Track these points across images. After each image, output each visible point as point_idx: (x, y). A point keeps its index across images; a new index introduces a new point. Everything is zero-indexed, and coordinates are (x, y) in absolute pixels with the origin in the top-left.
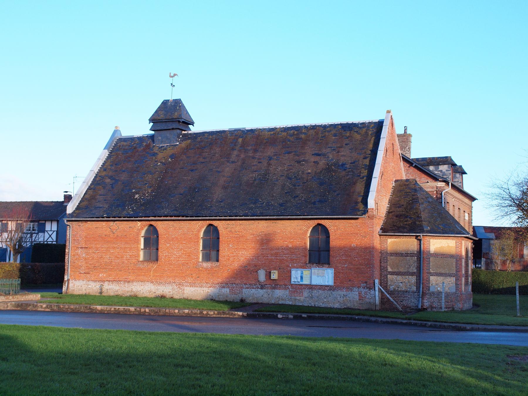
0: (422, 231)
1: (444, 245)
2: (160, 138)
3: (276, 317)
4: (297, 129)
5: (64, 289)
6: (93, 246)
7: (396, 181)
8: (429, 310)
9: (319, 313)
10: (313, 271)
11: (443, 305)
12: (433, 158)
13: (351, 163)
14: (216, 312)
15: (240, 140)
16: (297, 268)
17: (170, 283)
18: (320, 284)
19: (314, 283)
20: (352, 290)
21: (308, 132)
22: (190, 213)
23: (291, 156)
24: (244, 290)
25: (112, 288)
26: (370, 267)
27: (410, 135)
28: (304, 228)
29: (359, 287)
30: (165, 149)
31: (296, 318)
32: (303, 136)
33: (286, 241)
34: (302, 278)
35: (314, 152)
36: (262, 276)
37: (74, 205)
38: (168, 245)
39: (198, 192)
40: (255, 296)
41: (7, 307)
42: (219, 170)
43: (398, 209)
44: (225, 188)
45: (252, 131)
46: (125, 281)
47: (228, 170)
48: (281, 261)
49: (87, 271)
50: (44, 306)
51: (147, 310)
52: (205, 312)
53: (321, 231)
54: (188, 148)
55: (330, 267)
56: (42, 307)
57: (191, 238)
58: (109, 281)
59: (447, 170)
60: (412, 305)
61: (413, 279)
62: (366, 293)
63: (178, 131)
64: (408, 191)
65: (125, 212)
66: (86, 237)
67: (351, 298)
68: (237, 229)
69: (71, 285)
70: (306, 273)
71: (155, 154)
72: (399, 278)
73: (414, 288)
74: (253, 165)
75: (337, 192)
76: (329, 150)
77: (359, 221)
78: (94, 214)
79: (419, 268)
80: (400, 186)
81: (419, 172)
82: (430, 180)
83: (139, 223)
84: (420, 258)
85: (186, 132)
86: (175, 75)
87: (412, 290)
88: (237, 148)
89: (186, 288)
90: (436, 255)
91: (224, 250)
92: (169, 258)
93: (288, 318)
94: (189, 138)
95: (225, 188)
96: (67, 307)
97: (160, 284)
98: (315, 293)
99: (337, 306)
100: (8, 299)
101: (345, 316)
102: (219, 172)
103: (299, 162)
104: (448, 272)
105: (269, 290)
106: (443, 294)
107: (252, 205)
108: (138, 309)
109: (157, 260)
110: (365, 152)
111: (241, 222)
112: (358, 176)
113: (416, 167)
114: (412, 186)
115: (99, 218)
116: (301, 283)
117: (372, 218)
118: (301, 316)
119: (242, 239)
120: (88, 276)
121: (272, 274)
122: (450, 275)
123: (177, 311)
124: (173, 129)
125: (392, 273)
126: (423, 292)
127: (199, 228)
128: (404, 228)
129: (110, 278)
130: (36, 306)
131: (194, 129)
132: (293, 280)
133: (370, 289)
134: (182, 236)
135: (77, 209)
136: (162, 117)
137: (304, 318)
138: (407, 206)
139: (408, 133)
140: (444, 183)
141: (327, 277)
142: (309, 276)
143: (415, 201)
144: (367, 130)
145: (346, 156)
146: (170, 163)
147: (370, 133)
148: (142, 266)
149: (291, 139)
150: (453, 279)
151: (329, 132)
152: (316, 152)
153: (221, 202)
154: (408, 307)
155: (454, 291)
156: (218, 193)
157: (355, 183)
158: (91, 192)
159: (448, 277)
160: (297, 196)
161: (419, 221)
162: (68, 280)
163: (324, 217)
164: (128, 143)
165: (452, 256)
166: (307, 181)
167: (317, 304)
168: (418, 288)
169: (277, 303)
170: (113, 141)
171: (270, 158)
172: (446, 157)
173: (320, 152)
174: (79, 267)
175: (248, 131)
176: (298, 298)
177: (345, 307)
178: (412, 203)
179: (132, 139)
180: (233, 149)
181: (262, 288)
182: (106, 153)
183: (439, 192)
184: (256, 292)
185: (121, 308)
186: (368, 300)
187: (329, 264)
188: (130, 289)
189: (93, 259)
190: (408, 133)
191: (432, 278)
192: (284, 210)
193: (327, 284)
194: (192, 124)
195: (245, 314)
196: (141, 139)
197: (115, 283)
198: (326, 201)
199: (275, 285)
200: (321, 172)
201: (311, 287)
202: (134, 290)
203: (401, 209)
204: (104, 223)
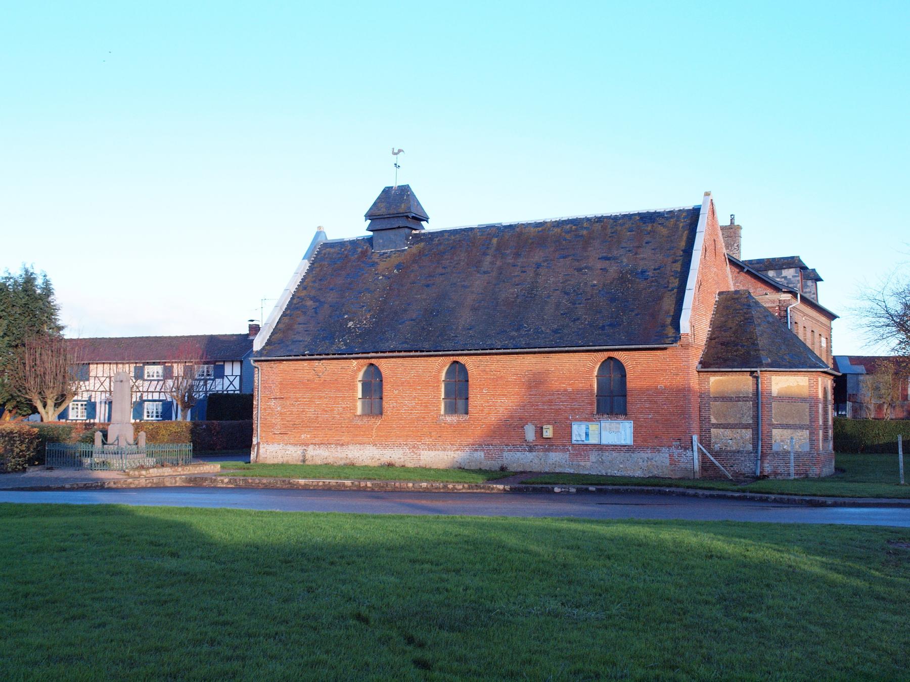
0: (760, 364)
3: (551, 492)
4: (576, 223)
5: (253, 456)
6: (292, 395)
7: (720, 294)
8: (772, 477)
12: (774, 259)
14: (466, 486)
15: (495, 241)
18: (614, 443)
19: (604, 442)
20: (659, 451)
23: (568, 261)
25: (319, 454)
27: (739, 227)
28: (589, 364)
30: (389, 257)
31: (580, 492)
32: (585, 232)
34: (587, 435)
36: (530, 433)
37: (264, 339)
38: (396, 392)
39: (436, 315)
41: (176, 482)
42: (466, 283)
44: (474, 309)
45: (511, 227)
46: (337, 444)
47: (478, 282)
49: (283, 431)
50: (226, 480)
52: (450, 486)
53: (614, 368)
54: (421, 253)
56: (222, 482)
58: (315, 444)
61: (748, 434)
62: (679, 455)
63: (407, 230)
66: (281, 383)
67: (658, 462)
69: (262, 451)
70: (593, 427)
72: (728, 432)
73: (750, 447)
76: (622, 251)
79: (756, 418)
80: (727, 300)
81: (753, 280)
82: (769, 291)
83: (355, 362)
84: (758, 403)
85: (417, 232)
86: (400, 151)
88: (491, 251)
90: (781, 398)
91: (476, 398)
93: (568, 493)
95: (474, 309)
97: (385, 447)
98: (607, 456)
99: (638, 474)
102: (464, 287)
105: (541, 454)
108: (356, 483)
110: (675, 254)
111: (498, 357)
113: (748, 272)
114: (744, 301)
115: (315, 353)
118: (587, 489)
119: (501, 381)
120: (286, 437)
121: (544, 431)
122: (801, 427)
123: (410, 485)
124: (399, 227)
127: (437, 368)
128: (734, 360)
129: (316, 440)
131: (428, 227)
132: (574, 438)
133: (686, 449)
136: (383, 211)
137: (592, 492)
139: (736, 224)
140: (790, 295)
142: (597, 432)
144: (677, 221)
145: (648, 259)
146: (396, 275)
147: (681, 225)
148: (360, 423)
149: (568, 237)
150: (806, 433)
151: (622, 225)
152: (605, 255)
153: (470, 329)
155: (808, 449)
156: (465, 318)
157: (660, 298)
160: (578, 319)
161: (756, 350)
162: (258, 444)
163: (633, 347)
164: (337, 249)
166: (592, 295)
167: (610, 472)
168: (755, 446)
171: (538, 266)
173: (610, 255)
174: (273, 426)
175: (506, 227)
176: (582, 463)
180: (485, 254)
181: (530, 451)
182: (306, 265)
184: (523, 456)
185: (333, 482)
186: (682, 465)
187: (626, 414)
188: (344, 455)
189: (291, 414)
190: (736, 224)
191: (775, 432)
192: (560, 338)
193: (623, 443)
194: (426, 219)
195: (507, 487)
196: (354, 243)
197: (322, 447)
199: (549, 445)
200: (611, 283)
202: (350, 456)
204: (305, 364)
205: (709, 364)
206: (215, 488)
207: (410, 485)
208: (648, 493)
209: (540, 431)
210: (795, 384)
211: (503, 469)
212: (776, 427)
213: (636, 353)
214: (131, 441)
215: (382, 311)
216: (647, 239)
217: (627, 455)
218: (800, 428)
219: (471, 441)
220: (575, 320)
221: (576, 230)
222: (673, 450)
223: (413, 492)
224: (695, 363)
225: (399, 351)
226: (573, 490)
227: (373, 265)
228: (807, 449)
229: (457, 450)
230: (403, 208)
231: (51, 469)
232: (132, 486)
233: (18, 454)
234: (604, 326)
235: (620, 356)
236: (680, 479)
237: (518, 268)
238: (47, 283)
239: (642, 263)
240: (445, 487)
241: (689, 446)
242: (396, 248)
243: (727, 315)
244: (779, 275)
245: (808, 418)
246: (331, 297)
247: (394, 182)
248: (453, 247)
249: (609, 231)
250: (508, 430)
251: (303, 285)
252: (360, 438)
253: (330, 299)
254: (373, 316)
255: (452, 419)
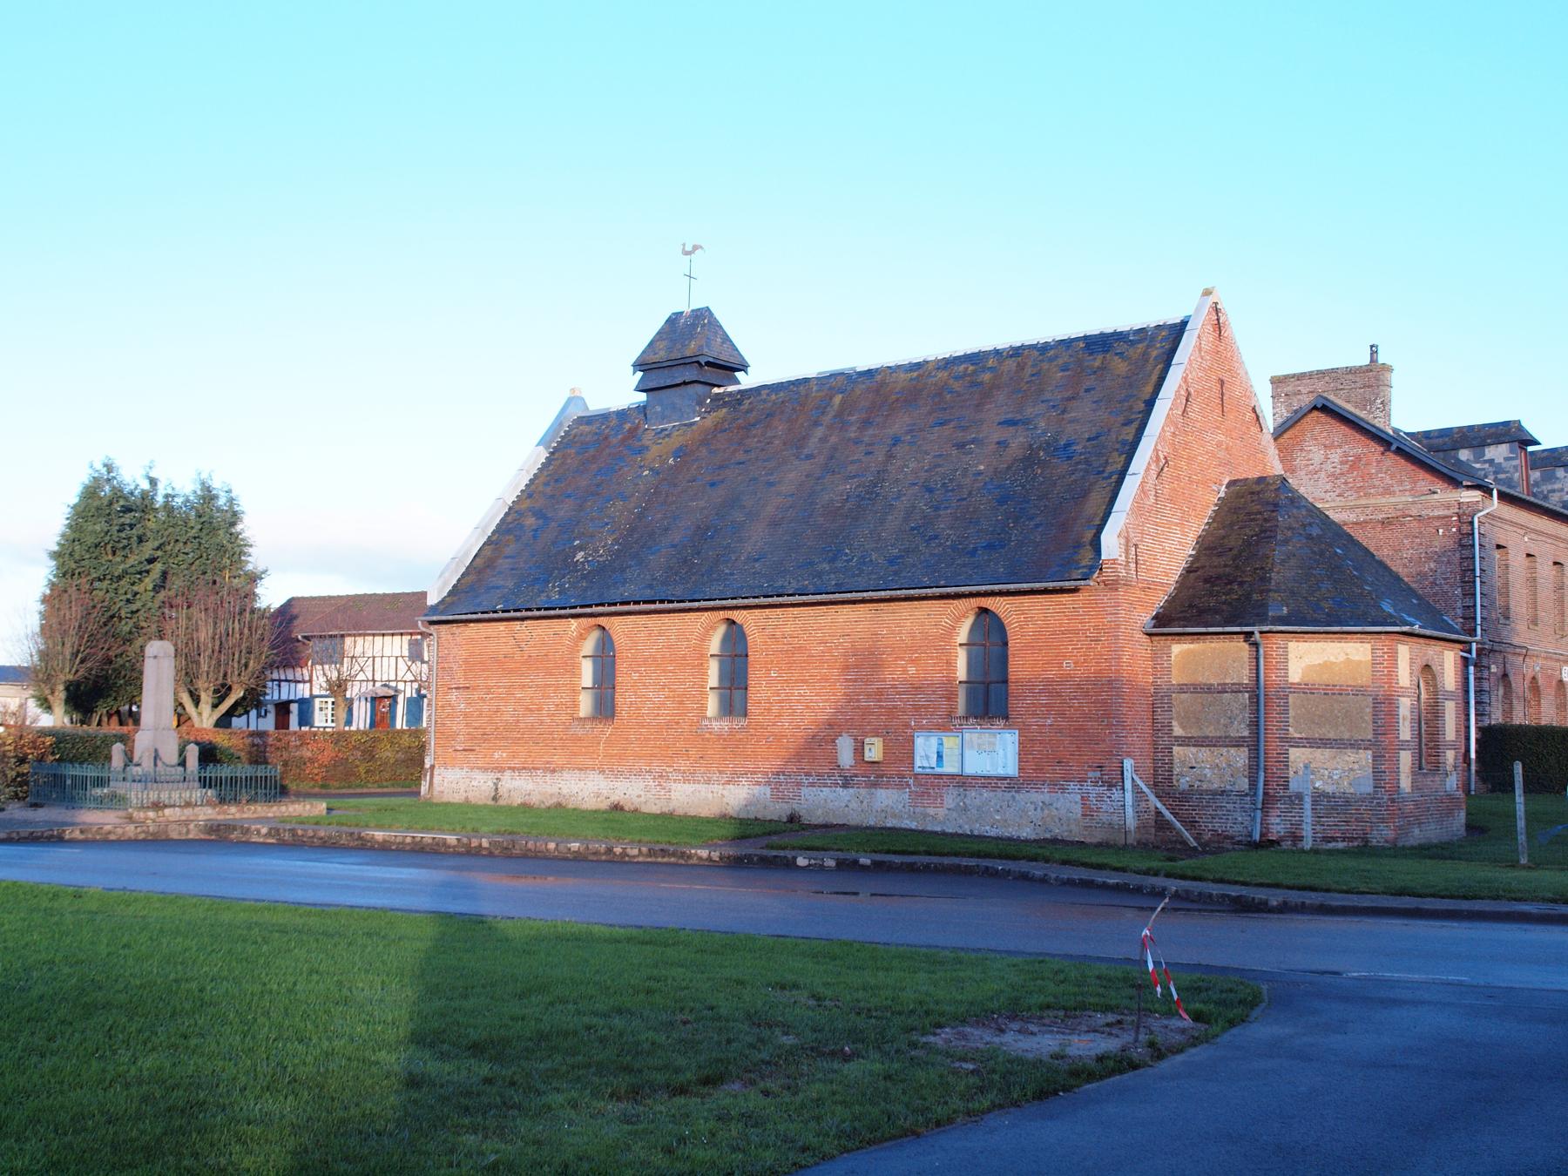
0: (1262, 619)
1: (1332, 659)
2: (659, 409)
3: (790, 865)
4: (975, 359)
5: (424, 789)
6: (480, 682)
7: (1231, 484)
8: (1287, 845)
9: (928, 853)
10: (967, 736)
11: (1307, 831)
12: (1471, 428)
13: (1089, 439)
14: (644, 850)
15: (838, 399)
16: (929, 729)
17: (639, 773)
18: (985, 773)
19: (969, 770)
20: (1063, 790)
21: (1000, 363)
22: (679, 591)
23: (947, 430)
24: (804, 791)
25: (521, 787)
26: (1110, 725)
27: (1387, 369)
28: (946, 621)
29: (1082, 781)
30: (668, 436)
31: (842, 865)
32: (986, 377)
33: (902, 659)
34: (940, 756)
35: (1003, 418)
36: (846, 757)
37: (445, 584)
38: (635, 676)
39: (712, 537)
40: (831, 805)
41: (188, 832)
42: (772, 478)
43: (1216, 561)
44: (774, 524)
45: (869, 373)
46: (545, 770)
47: (792, 476)
48: (891, 712)
49: (468, 745)
50: (264, 831)
51: (485, 843)
52: (618, 850)
53: (990, 630)
54: (718, 428)
55: (1008, 727)
56: (258, 832)
57: (684, 658)
58: (513, 769)
59: (1507, 459)
60: (1236, 830)
61: (1240, 757)
62: (1100, 798)
63: (699, 388)
64: (1256, 508)
65: (543, 597)
66: (466, 662)
67: (1058, 811)
68: (788, 629)
69: (436, 779)
70: (951, 742)
71: (643, 450)
72: (1204, 753)
73: (1244, 784)
74: (852, 462)
75: (1037, 520)
76: (1041, 408)
77: (1080, 596)
78: (479, 604)
79: (1255, 724)
80: (1239, 496)
81: (1410, 467)
82: (1439, 486)
83: (574, 623)
84: (1258, 696)
85: (721, 390)
86: (696, 248)
87: (1237, 788)
88: (827, 419)
89: (674, 786)
90: (1306, 689)
91: (760, 688)
92: (638, 709)
93: (822, 868)
94: (725, 404)
95: (774, 524)
96: (310, 833)
97: (617, 775)
98: (974, 797)
99: (1026, 833)
100: (225, 813)
101: (972, 862)
102: (771, 484)
103: (961, 446)
104: (1346, 736)
105: (863, 791)
106: (1308, 801)
107: (826, 566)
108: (465, 840)
109: (613, 716)
110: (1131, 408)
111: (796, 610)
112: (1099, 473)
113: (1400, 452)
114: (1269, 496)
115: (515, 612)
116: (939, 770)
117: (1112, 585)
118: (856, 862)
119: (810, 651)
120: (471, 756)
121: (867, 748)
122: (1354, 745)
123: (552, 846)
124: (685, 383)
125: (1185, 741)
126: (1265, 794)
127: (703, 633)
128: (1216, 611)
129: (516, 763)
130: (248, 829)
131: (746, 381)
132: (918, 763)
133: (1111, 786)
134: (673, 648)
135: (450, 593)
136: (662, 355)
137: (864, 867)
138: (1240, 552)
139: (1381, 361)
140: (1477, 493)
141: (1001, 752)
142: (957, 752)
143: (1266, 534)
144: (1148, 347)
145: (1083, 419)
146: (671, 467)
147: (1155, 353)
148: (580, 732)
149: (956, 386)
150: (1366, 757)
151: (1051, 360)
152: (1010, 416)
153: (756, 560)
154: (1227, 837)
155: (1370, 790)
156: (756, 537)
157: (1085, 494)
158: (488, 552)
159: (1349, 751)
160: (936, 537)
161: (1261, 592)
162: (432, 767)
163: (1025, 586)
164: (594, 428)
165: (1359, 691)
166: (970, 493)
167: (979, 829)
168: (1253, 783)
169: (881, 824)
170: (561, 424)
171: (896, 441)
172: (1506, 424)
173: (1019, 417)
174: (453, 736)
175: (861, 374)
176: (931, 811)
177: (1048, 836)
178: (1257, 543)
179: (604, 417)
180: (816, 424)
181: (845, 786)
182: (542, 455)
183: (1465, 518)
184: (832, 796)
185: (428, 837)
186: (1104, 818)
187: (1006, 718)
188: (555, 790)
189: (480, 715)
190: (1381, 361)
191: (1297, 755)
192: (896, 573)
193: (1001, 772)
194: (743, 367)
195: (715, 855)
196: (622, 415)
197: (524, 773)
198: (1003, 547)
199: (874, 775)
200: (1009, 468)
201: (962, 781)
202: (565, 791)
203: (1222, 561)
204: (501, 626)
205: (1176, 618)
206: (248, 843)
207: (552, 846)
208: (968, 871)
209: (859, 750)
210: (1342, 658)
211: (793, 818)
212: (1297, 743)
213: (1026, 600)
214: (175, 759)
215: (632, 530)
216: (1088, 384)
217: (1008, 796)
218: (1352, 746)
219: (765, 766)
220: (931, 539)
221: (974, 372)
222: (1088, 787)
223: (555, 858)
224: (1145, 617)
225: (662, 602)
226: (831, 863)
227: (640, 452)
228: (1367, 788)
229: (728, 783)
230: (692, 348)
231: (35, 805)
232: (112, 837)
233: (14, 780)
234: (975, 550)
235: (997, 605)
236: (1099, 845)
237: (862, 448)
238: (231, 501)
239: (1070, 428)
240: (609, 850)
241: (1114, 781)
242: (692, 417)
243: (1232, 524)
244: (1477, 459)
245: (1371, 727)
246: (565, 510)
247: (684, 304)
248: (770, 415)
249: (1028, 371)
250: (814, 751)
251: (529, 492)
252: (580, 759)
253: (562, 513)
254: (616, 541)
255: (723, 725)
